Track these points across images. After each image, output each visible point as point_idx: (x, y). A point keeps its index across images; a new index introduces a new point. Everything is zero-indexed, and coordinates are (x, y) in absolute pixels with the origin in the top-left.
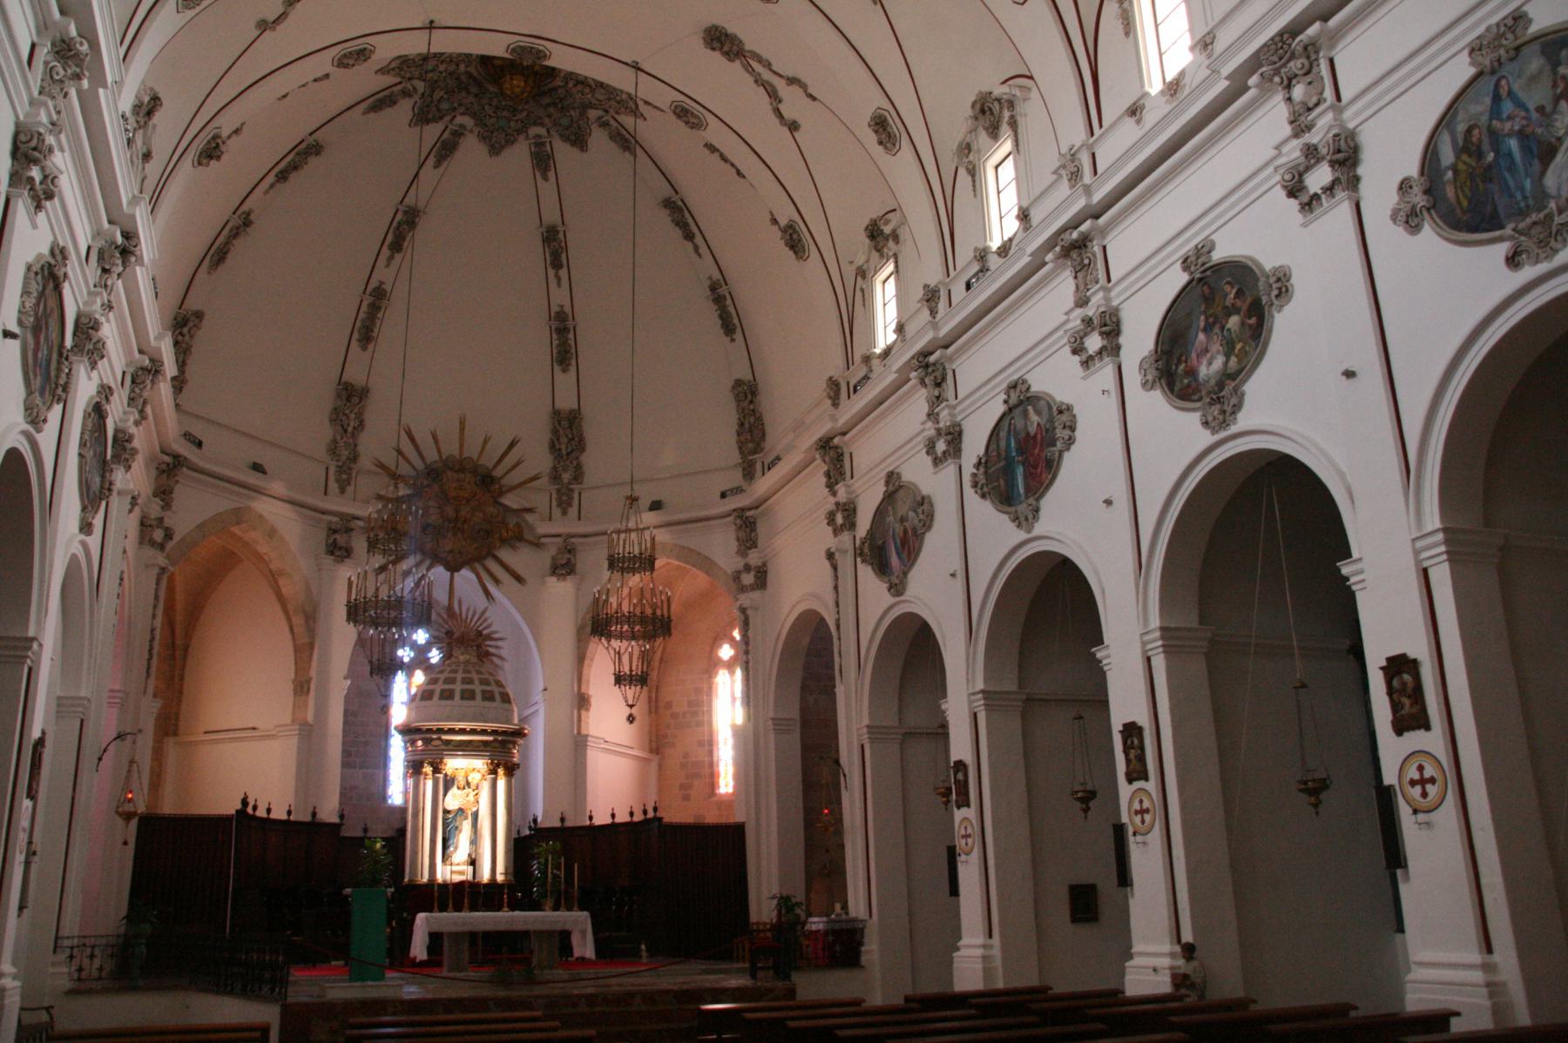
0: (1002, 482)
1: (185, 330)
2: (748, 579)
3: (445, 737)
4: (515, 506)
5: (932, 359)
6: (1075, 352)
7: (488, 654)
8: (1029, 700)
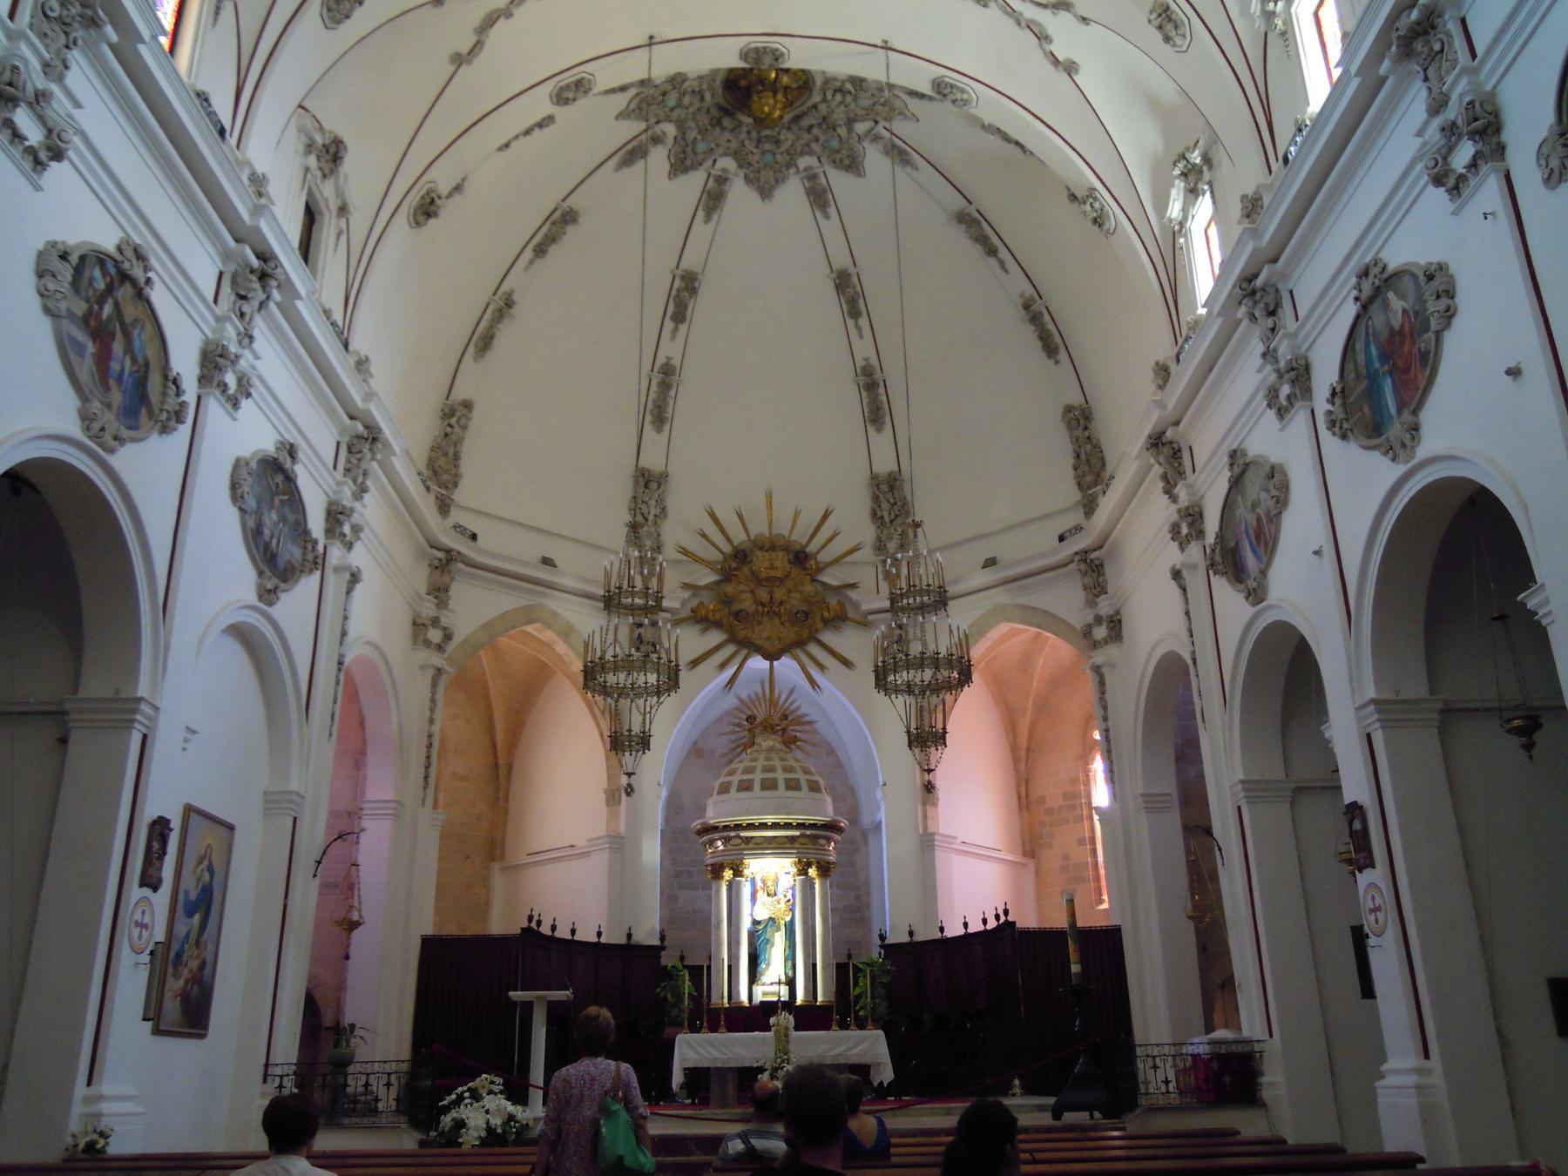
0: (1366, 409)
1: (453, 421)
2: (1100, 632)
3: (743, 834)
4: (834, 582)
5: (1259, 282)
7: (796, 739)
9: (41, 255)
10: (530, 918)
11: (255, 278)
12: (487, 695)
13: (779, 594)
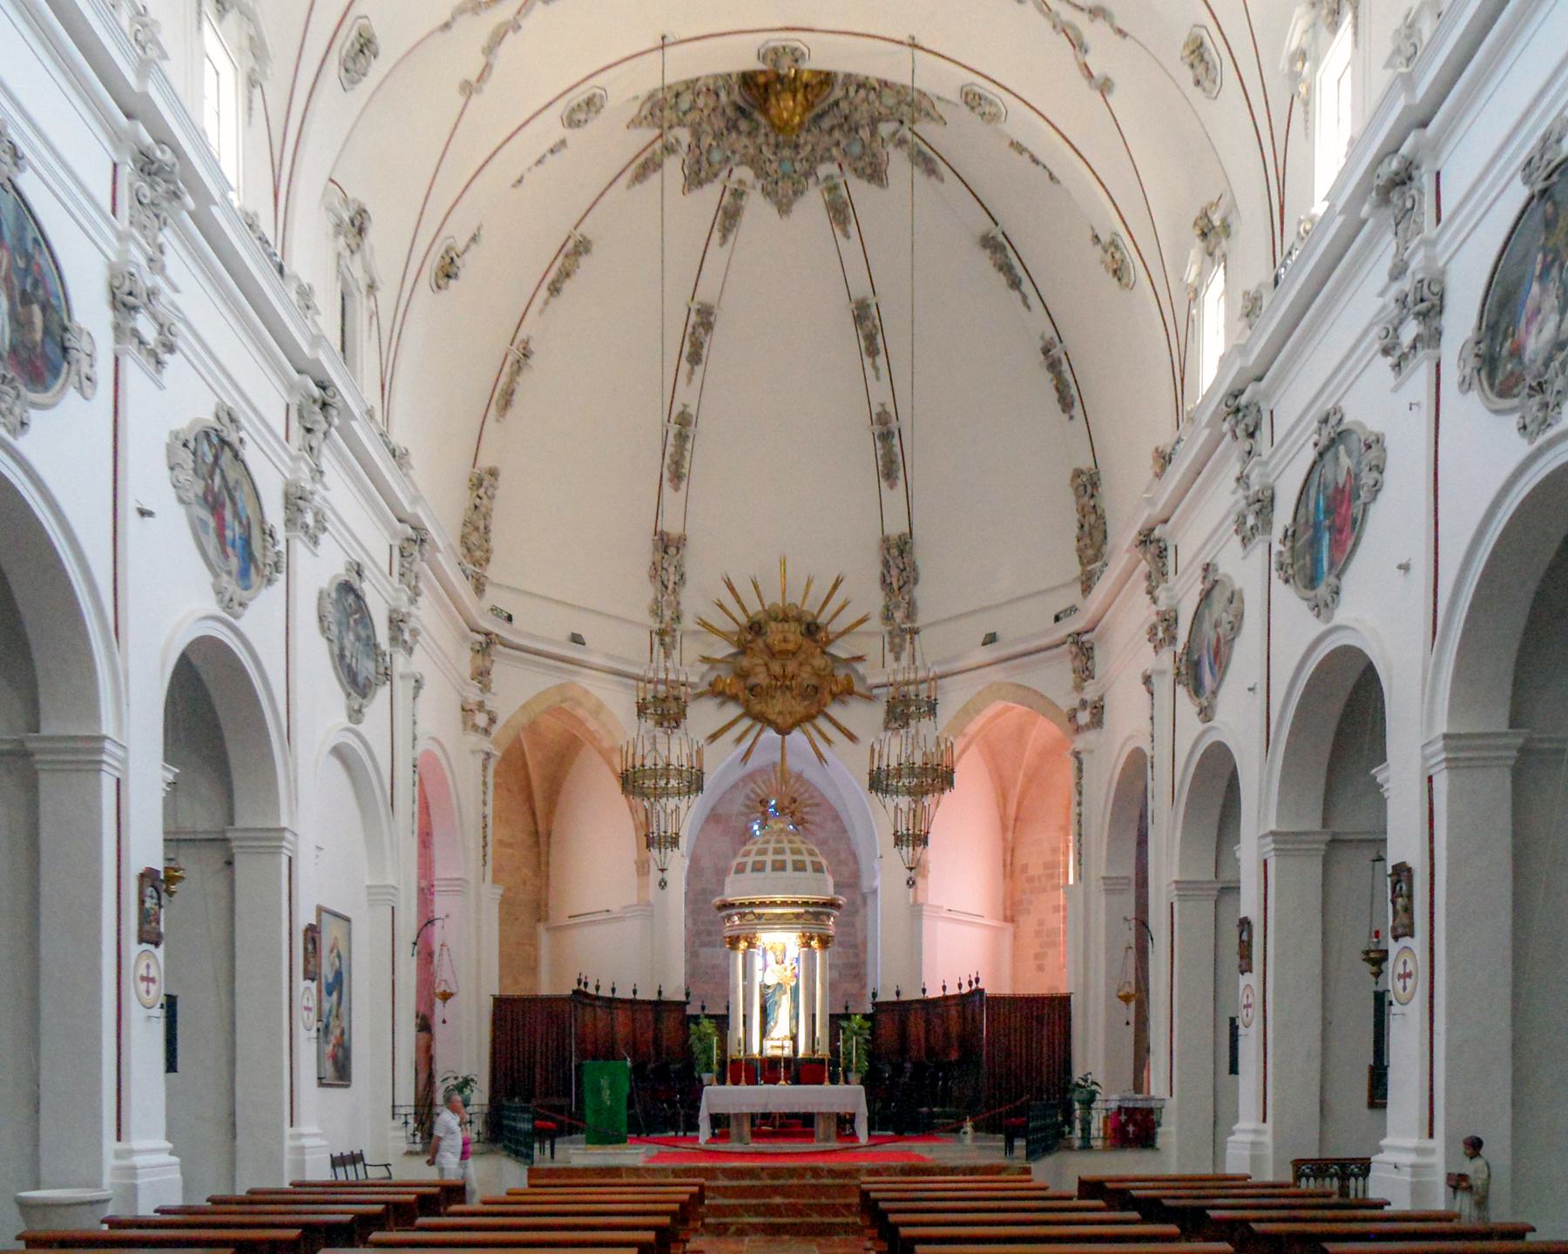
1: (481, 492)
2: (1084, 717)
3: (757, 911)
4: (843, 655)
5: (1243, 400)
6: (1386, 352)
8: (1335, 842)
9: (170, 449)
10: (579, 982)
11: (317, 408)
12: (525, 765)
13: (791, 667)
